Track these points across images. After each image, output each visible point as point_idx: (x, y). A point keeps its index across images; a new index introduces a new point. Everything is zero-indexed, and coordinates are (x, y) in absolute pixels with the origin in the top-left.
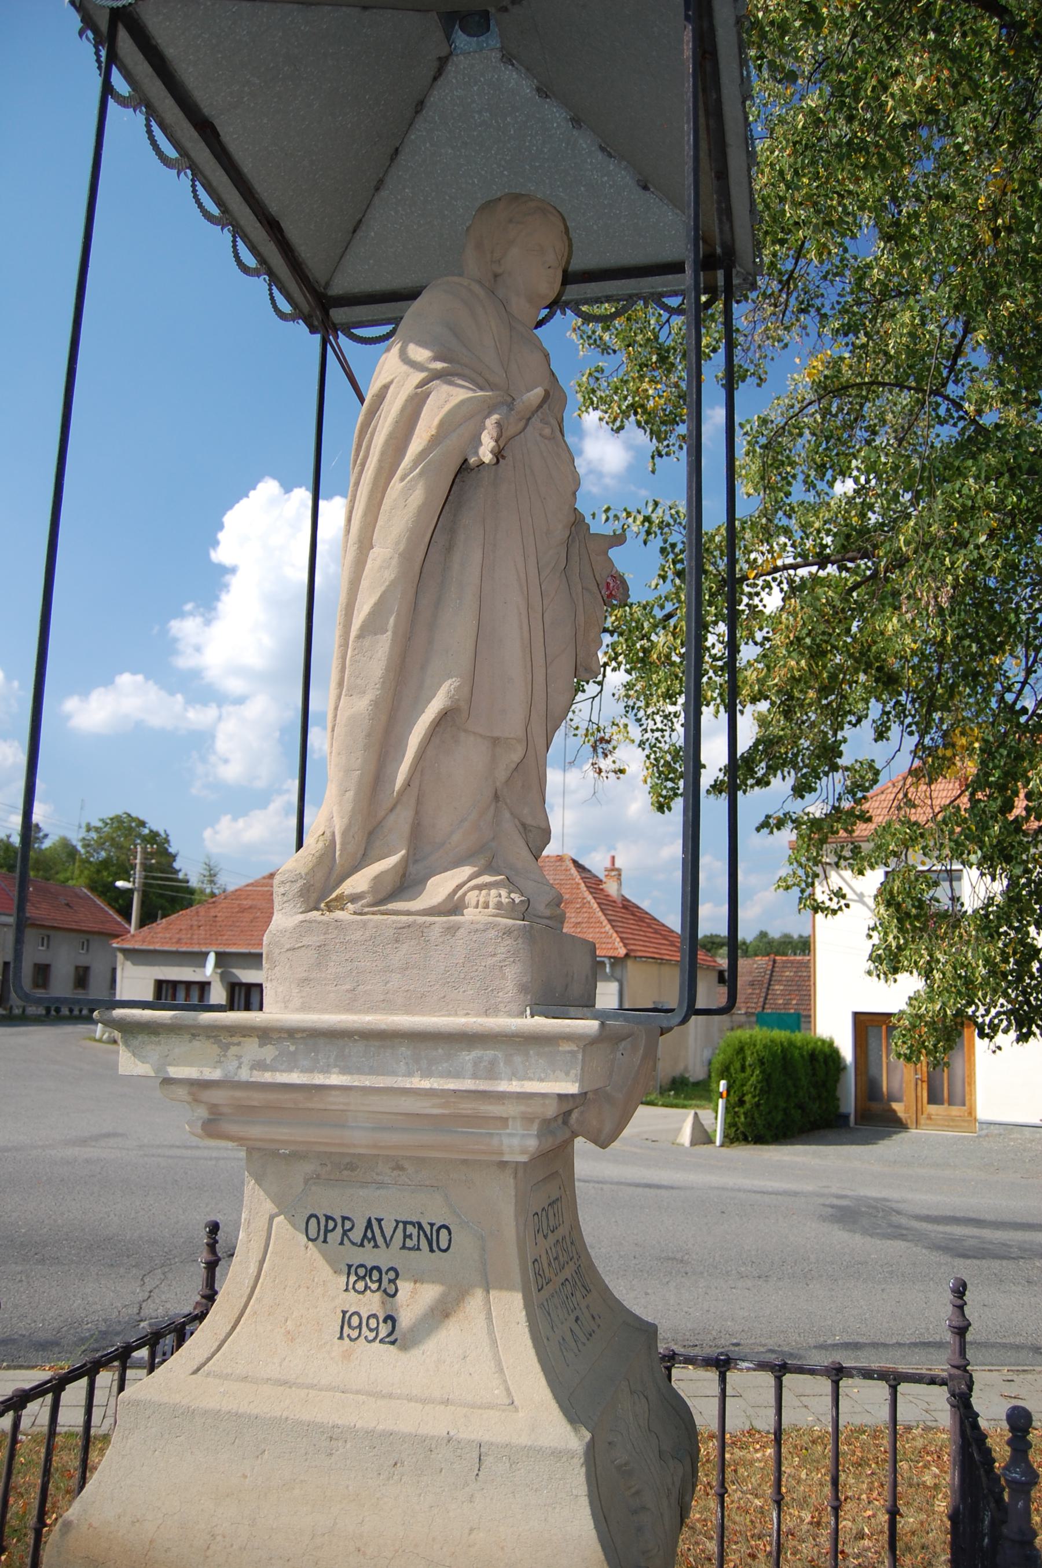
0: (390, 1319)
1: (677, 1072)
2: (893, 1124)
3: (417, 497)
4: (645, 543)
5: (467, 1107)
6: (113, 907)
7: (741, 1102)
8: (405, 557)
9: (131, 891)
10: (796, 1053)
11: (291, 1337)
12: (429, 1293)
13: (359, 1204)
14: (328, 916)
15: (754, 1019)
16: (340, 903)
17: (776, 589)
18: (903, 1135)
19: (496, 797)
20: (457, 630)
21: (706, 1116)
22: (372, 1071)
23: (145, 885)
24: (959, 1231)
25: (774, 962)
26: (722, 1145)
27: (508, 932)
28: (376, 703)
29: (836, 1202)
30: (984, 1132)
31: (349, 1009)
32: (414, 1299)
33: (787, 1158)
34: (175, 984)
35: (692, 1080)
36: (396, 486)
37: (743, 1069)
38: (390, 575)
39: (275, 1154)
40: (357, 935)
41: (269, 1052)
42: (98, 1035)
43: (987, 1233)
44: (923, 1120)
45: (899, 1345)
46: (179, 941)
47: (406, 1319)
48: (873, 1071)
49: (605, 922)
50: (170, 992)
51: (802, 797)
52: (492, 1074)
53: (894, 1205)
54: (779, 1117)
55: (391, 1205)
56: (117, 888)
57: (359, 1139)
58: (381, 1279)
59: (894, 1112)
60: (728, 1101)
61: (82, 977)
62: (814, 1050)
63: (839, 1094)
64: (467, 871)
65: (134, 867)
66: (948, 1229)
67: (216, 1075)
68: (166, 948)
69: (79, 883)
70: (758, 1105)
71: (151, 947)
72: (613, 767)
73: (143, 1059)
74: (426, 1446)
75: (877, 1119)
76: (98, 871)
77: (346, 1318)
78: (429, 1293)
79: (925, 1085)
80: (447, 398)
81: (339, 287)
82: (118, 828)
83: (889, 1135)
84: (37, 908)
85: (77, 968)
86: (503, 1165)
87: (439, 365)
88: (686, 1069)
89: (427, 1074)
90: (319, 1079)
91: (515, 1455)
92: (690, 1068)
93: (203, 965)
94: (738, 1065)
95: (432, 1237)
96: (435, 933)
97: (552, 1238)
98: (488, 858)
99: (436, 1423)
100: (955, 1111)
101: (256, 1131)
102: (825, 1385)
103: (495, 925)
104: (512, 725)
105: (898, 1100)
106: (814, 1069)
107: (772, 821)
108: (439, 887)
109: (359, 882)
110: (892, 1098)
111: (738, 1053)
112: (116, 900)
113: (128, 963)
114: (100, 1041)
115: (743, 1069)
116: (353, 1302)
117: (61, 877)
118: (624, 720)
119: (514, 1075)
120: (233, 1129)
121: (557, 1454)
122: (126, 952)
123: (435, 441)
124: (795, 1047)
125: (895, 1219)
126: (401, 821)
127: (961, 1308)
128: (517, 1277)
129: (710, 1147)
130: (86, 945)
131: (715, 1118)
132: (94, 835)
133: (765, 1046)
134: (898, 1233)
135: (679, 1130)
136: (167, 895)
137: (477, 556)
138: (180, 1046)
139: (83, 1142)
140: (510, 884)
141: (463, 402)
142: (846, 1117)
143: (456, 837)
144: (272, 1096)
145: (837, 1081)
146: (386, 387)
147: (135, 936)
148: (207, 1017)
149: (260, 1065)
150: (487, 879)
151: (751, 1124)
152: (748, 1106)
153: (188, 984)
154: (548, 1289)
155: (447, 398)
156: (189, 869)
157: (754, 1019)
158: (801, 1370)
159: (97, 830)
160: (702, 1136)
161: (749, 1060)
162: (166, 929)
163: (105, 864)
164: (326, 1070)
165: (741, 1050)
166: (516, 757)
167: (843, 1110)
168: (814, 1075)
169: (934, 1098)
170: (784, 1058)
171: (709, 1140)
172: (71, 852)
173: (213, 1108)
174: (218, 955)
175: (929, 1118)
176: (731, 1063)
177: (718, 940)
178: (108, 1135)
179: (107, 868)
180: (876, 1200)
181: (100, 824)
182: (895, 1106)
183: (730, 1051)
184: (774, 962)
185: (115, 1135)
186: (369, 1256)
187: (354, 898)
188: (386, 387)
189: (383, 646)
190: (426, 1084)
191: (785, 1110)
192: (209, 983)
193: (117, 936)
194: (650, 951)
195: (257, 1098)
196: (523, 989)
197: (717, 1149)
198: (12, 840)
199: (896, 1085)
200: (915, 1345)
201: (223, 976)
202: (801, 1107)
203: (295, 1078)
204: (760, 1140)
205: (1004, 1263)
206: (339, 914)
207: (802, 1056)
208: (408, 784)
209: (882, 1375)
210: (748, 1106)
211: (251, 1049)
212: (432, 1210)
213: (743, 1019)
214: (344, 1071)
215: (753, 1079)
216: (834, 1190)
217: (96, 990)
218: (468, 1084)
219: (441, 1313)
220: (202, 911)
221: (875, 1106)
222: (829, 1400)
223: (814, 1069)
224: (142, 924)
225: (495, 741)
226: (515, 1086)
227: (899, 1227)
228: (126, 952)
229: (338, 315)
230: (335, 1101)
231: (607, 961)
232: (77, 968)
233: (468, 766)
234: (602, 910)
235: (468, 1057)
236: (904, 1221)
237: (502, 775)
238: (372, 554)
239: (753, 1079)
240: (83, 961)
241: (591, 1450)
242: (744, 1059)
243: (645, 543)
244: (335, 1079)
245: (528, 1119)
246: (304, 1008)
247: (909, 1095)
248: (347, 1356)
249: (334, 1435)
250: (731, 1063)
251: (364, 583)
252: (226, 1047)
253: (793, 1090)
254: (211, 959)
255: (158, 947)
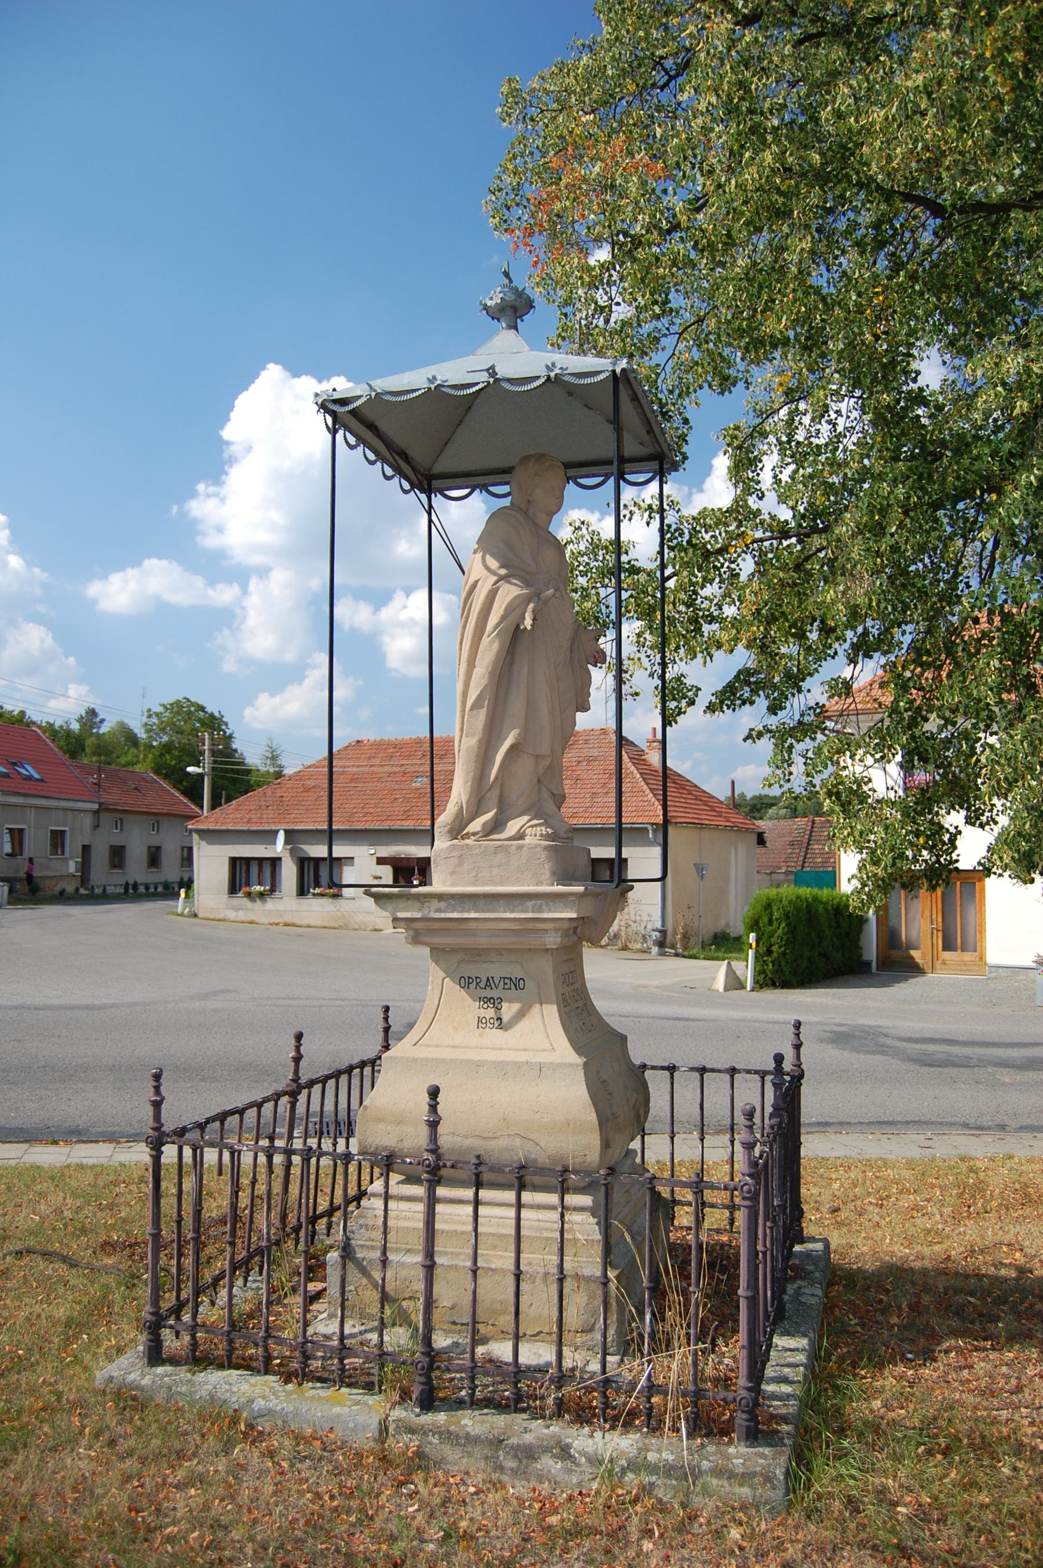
0: (499, 1019)
1: (719, 927)
2: (913, 969)
3: (496, 646)
4: (648, 524)
5: (530, 925)
6: (178, 789)
7: (769, 952)
8: (492, 673)
9: (201, 776)
10: (821, 908)
11: (456, 1029)
12: (516, 1007)
13: (483, 971)
14: (463, 842)
15: (792, 877)
16: (468, 836)
17: (748, 557)
18: (920, 979)
19: (539, 781)
20: (517, 706)
21: (738, 966)
22: (489, 911)
23: (213, 769)
24: (931, 1048)
25: (813, 822)
26: (752, 990)
27: (546, 848)
28: (480, 741)
29: (835, 1029)
30: (993, 975)
31: (474, 885)
32: (509, 1010)
33: (808, 1000)
34: (248, 861)
35: (733, 935)
36: (485, 640)
37: (770, 922)
38: (484, 682)
39: (443, 950)
40: (477, 851)
41: (443, 905)
42: (179, 910)
43: (956, 1050)
44: (938, 965)
45: (860, 1123)
46: (249, 821)
47: (505, 1018)
48: (893, 922)
49: (648, 791)
50: (244, 868)
51: (776, 714)
52: (540, 911)
53: (884, 1031)
54: (804, 964)
55: (497, 970)
56: (189, 774)
57: (483, 941)
58: (495, 1003)
59: (912, 958)
60: (757, 951)
61: (154, 858)
62: (839, 905)
63: (861, 943)
64: (526, 818)
65: (202, 753)
66: (924, 1047)
67: (419, 915)
68: (238, 828)
69: (144, 768)
70: (784, 954)
71: (224, 828)
72: (630, 691)
73: (385, 910)
74: (518, 1065)
75: (897, 963)
76: (162, 755)
77: (479, 1020)
78: (516, 1007)
79: (940, 934)
80: (510, 592)
81: (437, 469)
82: (178, 713)
83: (906, 979)
84: (109, 794)
85: (149, 848)
86: (547, 950)
87: (503, 572)
88: (727, 925)
89: (513, 911)
90: (466, 915)
91: (554, 1067)
92: (731, 924)
93: (274, 843)
94: (766, 919)
95: (517, 984)
96: (513, 849)
97: (571, 988)
98: (536, 811)
99: (522, 1057)
100: (967, 956)
101: (437, 940)
102: (727, 1077)
103: (539, 845)
104: (545, 749)
105: (917, 948)
106: (837, 922)
107: (754, 733)
108: (513, 827)
109: (476, 826)
110: (911, 946)
111: (766, 909)
112: (181, 782)
113: (204, 843)
114: (182, 915)
115: (770, 922)
116: (482, 1013)
117: (122, 760)
118: (638, 655)
119: (550, 911)
120: (427, 940)
121: (572, 1065)
122: (200, 832)
123: (503, 618)
124: (821, 902)
125: (881, 1040)
126: (494, 795)
127: (798, 1035)
128: (554, 998)
129: (742, 992)
130: (157, 826)
131: (746, 969)
132: (155, 720)
133: (790, 902)
134: (883, 1050)
135: (714, 979)
136: (234, 780)
137: (525, 669)
138: (402, 904)
139: (206, 997)
140: (547, 824)
141: (516, 597)
142: (868, 964)
143: (520, 802)
144: (444, 925)
145: (860, 931)
146: (477, 582)
147: (209, 818)
148: (414, 890)
149: (439, 910)
150: (535, 822)
151: (779, 971)
152: (775, 955)
153: (260, 860)
154: (569, 1008)
155: (510, 592)
156: (251, 753)
157: (792, 877)
158: (713, 1070)
159: (158, 715)
160: (735, 983)
161: (776, 915)
162: (237, 810)
163: (167, 748)
164: (468, 911)
165: (768, 906)
166: (547, 763)
167: (865, 957)
168: (838, 927)
169: (948, 945)
170: (809, 912)
171: (742, 986)
172: (132, 739)
173: (416, 931)
174: (286, 832)
175: (944, 963)
176: (760, 917)
177: (766, 801)
178: (222, 992)
179: (169, 752)
180: (870, 1027)
181: (161, 709)
182: (913, 953)
183: (759, 907)
184: (813, 822)
185: (228, 991)
186: (488, 993)
187: (474, 834)
188: (477, 582)
189: (482, 714)
190: (512, 916)
191: (809, 958)
192: (280, 859)
193: (192, 818)
194: (690, 817)
195: (436, 925)
196: (553, 873)
197: (747, 994)
198: (72, 727)
199: (914, 934)
200: (872, 1123)
201: (292, 852)
202: (824, 955)
203: (455, 915)
204: (786, 985)
205: (962, 1070)
206: (467, 841)
207: (826, 910)
208: (496, 778)
209: (756, 1072)
210: (775, 955)
211: (435, 904)
212: (516, 972)
213: (782, 877)
214: (477, 911)
215: (780, 931)
216: (837, 1021)
217: (170, 871)
218: (530, 915)
219: (521, 1015)
220: (269, 791)
221: (896, 954)
222: (729, 1084)
223: (837, 922)
224: (214, 806)
225: (537, 756)
226: (550, 915)
227: (884, 1046)
228: (200, 832)
229: (436, 484)
230: (472, 925)
231: (649, 827)
232: (149, 848)
233: (525, 767)
234: (644, 780)
235: (530, 904)
236: (888, 1041)
237: (541, 771)
238: (476, 670)
239: (780, 931)
240: (155, 841)
241: (585, 1064)
242: (771, 914)
243: (648, 524)
244: (473, 915)
245: (557, 930)
246: (453, 885)
247: (926, 943)
248: (481, 1035)
249: (479, 1064)
250: (760, 917)
251: (472, 685)
252: (423, 903)
253: (817, 941)
254: (281, 837)
255: (230, 827)
